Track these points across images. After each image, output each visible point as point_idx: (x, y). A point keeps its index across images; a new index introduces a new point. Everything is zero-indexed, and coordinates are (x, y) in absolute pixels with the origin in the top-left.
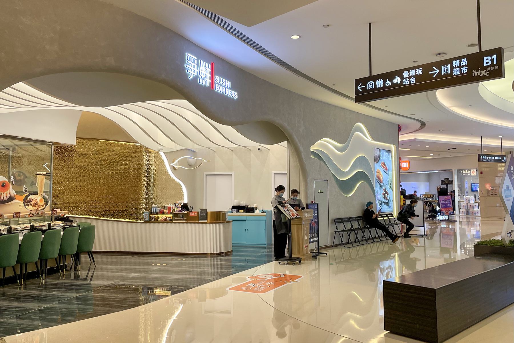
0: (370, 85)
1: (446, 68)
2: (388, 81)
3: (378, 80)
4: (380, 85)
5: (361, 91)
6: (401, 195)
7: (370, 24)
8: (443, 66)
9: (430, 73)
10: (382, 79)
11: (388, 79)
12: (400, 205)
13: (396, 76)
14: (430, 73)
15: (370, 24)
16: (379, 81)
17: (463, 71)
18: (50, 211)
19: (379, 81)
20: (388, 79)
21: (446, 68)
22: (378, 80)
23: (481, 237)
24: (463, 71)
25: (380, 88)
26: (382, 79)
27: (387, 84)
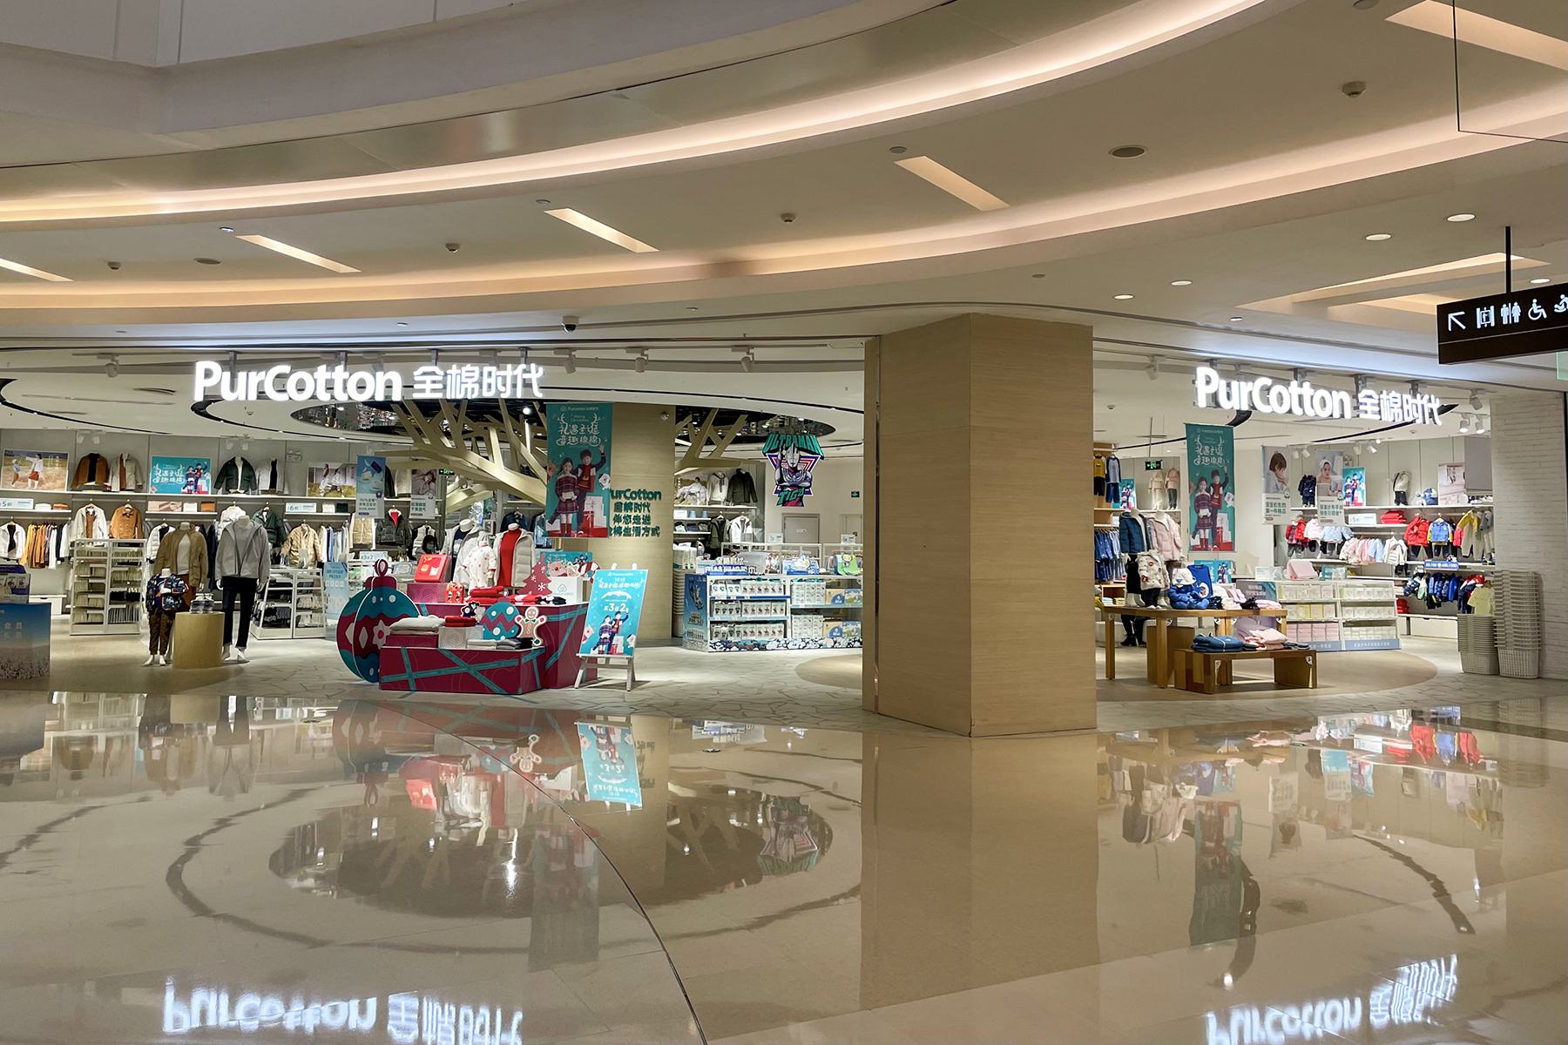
0: (1484, 317)
1: (1486, 313)
2: (1534, 305)
3: (1505, 305)
4: (1513, 318)
5: (1450, 329)
6: (595, 718)
7: (1508, 230)
8: (1478, 310)
9: (1464, 327)
10: (1516, 304)
11: (1535, 301)
12: (763, 531)
13: (1562, 296)
14: (1464, 327)
15: (1508, 230)
16: (1508, 306)
17: (466, 389)
18: (451, 497)
19: (1508, 306)
20: (1535, 301)
21: (1486, 313)
22: (1505, 305)
23: (296, 731)
24: (466, 389)
25: (1512, 326)
26: (1516, 304)
27: (1534, 315)
